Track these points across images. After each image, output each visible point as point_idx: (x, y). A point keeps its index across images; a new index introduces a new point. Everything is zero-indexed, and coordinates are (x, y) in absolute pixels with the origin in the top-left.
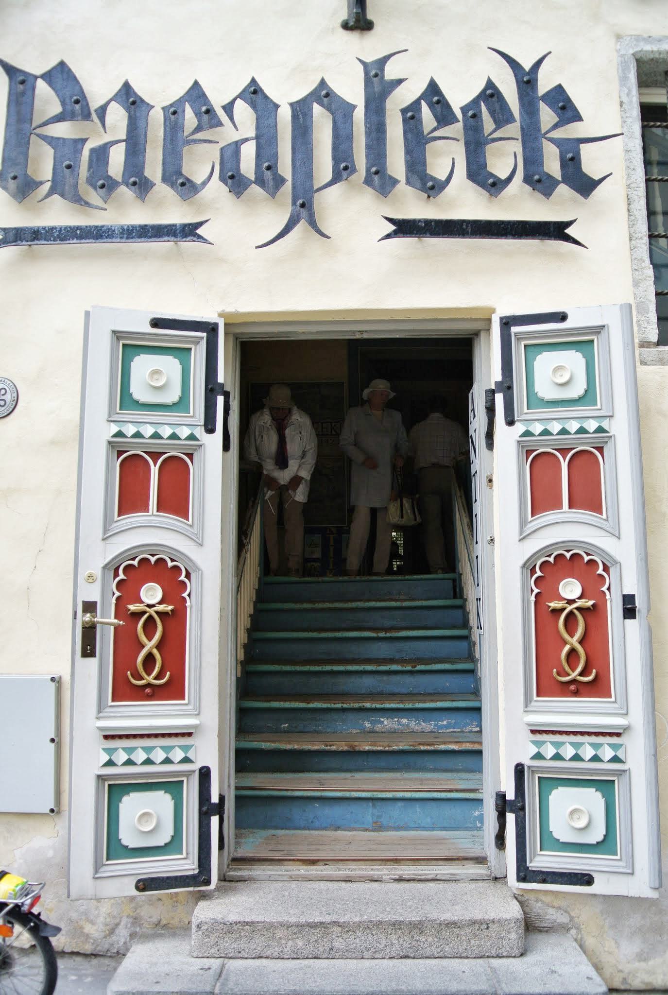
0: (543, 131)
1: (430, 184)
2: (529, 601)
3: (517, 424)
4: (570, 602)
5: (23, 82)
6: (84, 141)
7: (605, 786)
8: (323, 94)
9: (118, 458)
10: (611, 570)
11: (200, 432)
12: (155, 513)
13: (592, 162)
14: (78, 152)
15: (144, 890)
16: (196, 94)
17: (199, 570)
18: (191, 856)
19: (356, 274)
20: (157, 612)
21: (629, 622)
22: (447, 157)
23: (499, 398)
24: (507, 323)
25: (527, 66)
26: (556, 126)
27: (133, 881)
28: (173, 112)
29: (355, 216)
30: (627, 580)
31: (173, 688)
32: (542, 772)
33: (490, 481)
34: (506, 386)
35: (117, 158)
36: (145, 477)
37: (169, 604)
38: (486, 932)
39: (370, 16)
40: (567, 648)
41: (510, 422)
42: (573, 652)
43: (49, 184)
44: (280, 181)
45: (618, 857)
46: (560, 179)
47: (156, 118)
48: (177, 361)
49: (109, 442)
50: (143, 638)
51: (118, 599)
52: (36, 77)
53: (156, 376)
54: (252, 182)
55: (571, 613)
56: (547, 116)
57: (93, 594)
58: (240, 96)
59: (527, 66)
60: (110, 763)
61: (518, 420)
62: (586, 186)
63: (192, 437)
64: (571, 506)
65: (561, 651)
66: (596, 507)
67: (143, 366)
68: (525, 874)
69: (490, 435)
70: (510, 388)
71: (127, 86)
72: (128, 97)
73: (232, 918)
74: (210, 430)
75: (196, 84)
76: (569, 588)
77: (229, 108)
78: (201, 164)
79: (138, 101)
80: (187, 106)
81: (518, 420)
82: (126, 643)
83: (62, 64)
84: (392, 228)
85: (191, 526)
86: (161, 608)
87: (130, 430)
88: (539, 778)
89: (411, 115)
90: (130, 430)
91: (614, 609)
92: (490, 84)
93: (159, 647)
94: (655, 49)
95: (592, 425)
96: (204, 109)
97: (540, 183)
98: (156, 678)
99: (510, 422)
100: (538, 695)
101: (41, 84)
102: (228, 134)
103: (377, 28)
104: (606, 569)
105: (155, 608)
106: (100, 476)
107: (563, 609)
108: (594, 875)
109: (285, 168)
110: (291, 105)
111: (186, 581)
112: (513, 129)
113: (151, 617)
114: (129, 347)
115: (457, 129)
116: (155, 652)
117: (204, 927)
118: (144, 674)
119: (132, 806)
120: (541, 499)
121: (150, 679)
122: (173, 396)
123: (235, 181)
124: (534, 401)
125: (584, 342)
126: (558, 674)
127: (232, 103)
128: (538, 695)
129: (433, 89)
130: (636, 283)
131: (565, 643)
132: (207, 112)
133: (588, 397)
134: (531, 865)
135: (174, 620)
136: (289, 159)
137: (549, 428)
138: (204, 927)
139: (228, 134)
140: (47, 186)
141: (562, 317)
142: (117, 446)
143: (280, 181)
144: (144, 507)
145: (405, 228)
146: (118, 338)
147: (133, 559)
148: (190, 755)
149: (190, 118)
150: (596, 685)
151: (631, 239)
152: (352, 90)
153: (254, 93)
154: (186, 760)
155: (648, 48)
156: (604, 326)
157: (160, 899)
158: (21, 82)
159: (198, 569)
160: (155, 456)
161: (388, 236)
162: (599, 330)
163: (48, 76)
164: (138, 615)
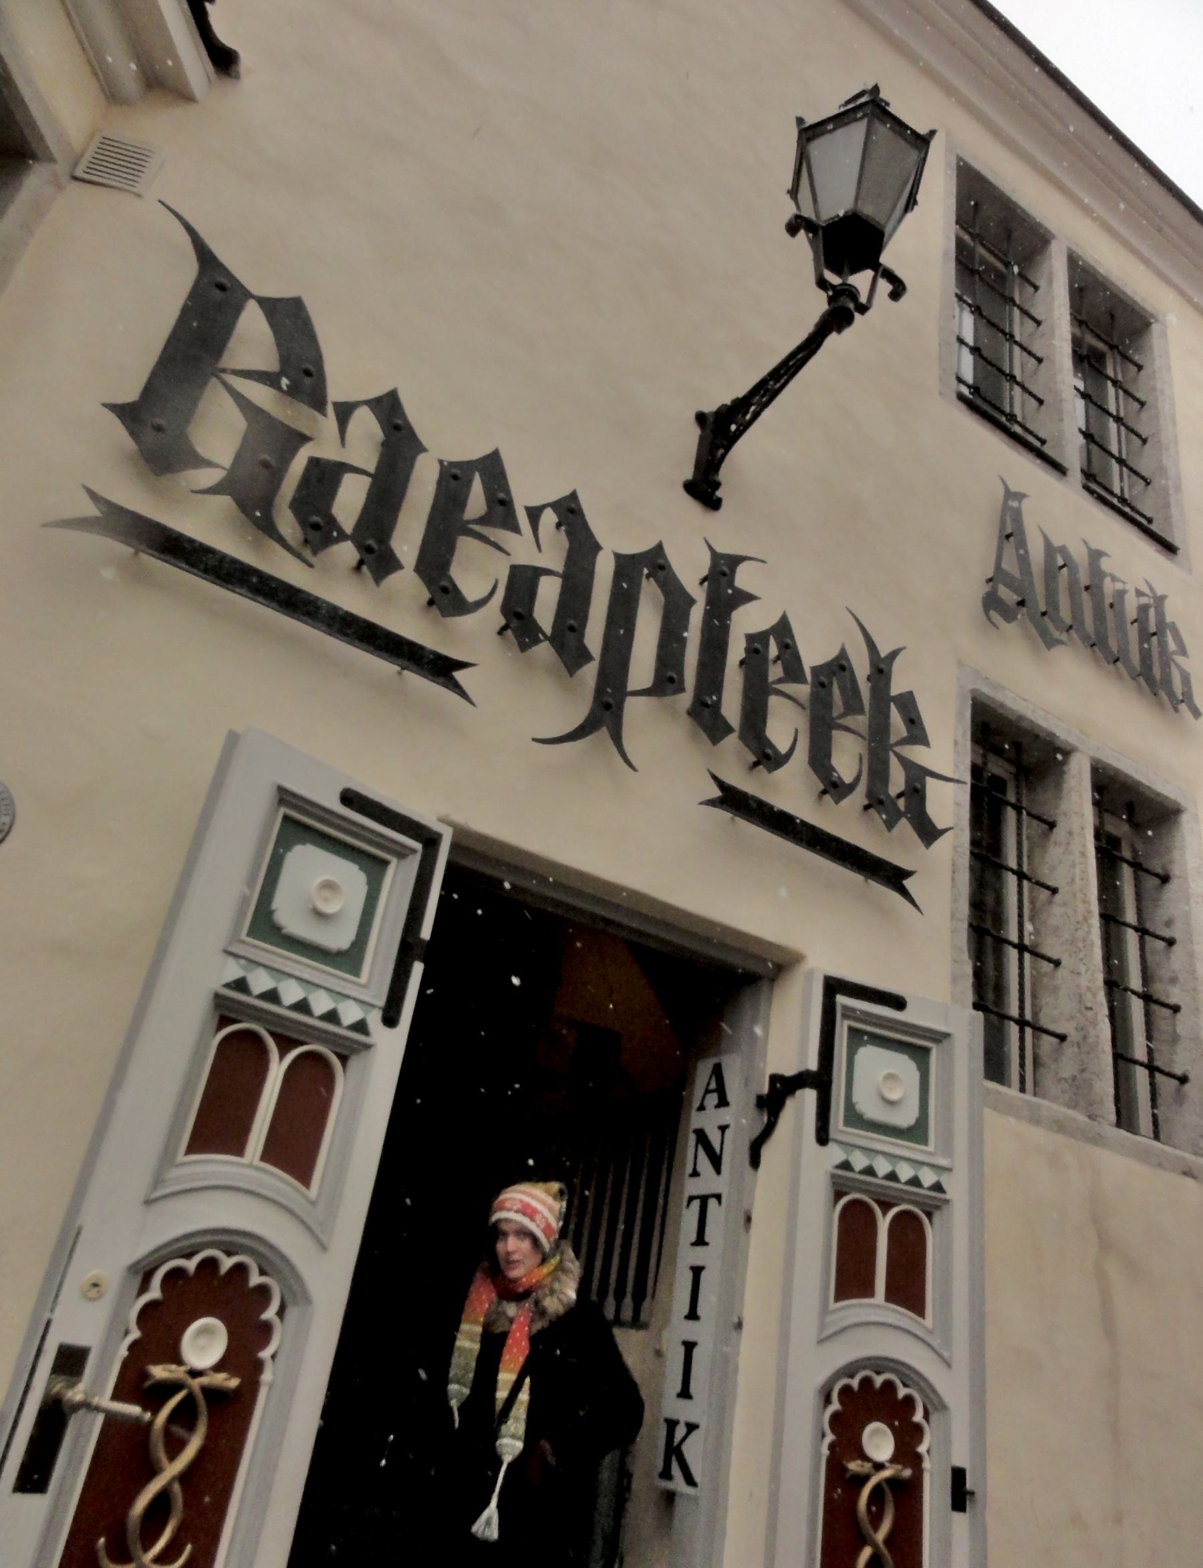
1: (316, 519)
3: (832, 1146)
4: (879, 1467)
6: (304, 439)
8: (655, 562)
9: (219, 1028)
11: (374, 1020)
12: (257, 1162)
14: (293, 451)
19: (637, 829)
21: (958, 1516)
22: (784, 725)
24: (833, 987)
26: (780, 681)
28: (454, 478)
33: (749, 1219)
35: (350, 499)
36: (252, 1083)
37: (233, 1374)
44: (583, 656)
47: (604, 568)
49: (217, 996)
50: (162, 1455)
52: (248, 295)
53: (327, 893)
54: (343, 536)
58: (367, 403)
61: (836, 1141)
63: (361, 1027)
64: (267, 1156)
65: (130, 1500)
74: (390, 1020)
77: (534, 514)
78: (477, 571)
81: (836, 1141)
82: (125, 1456)
84: (459, 675)
85: (313, 1203)
87: (260, 982)
90: (260, 982)
92: (843, 654)
93: (184, 1478)
102: (521, 549)
105: (204, 1380)
106: (174, 1058)
107: (865, 1478)
109: (594, 636)
110: (618, 557)
111: (276, 1321)
114: (298, 822)
115: (803, 691)
122: (340, 938)
123: (518, 621)
129: (783, 629)
133: (917, 1132)
135: (227, 1411)
139: (521, 549)
140: (208, 477)
141: (898, 1003)
142: (225, 1010)
143: (583, 656)
145: (733, 800)
147: (189, 1256)
149: (773, 650)
156: (947, 1035)
159: (308, 1300)
160: (285, 1044)
163: (270, 306)
164: (170, 1388)
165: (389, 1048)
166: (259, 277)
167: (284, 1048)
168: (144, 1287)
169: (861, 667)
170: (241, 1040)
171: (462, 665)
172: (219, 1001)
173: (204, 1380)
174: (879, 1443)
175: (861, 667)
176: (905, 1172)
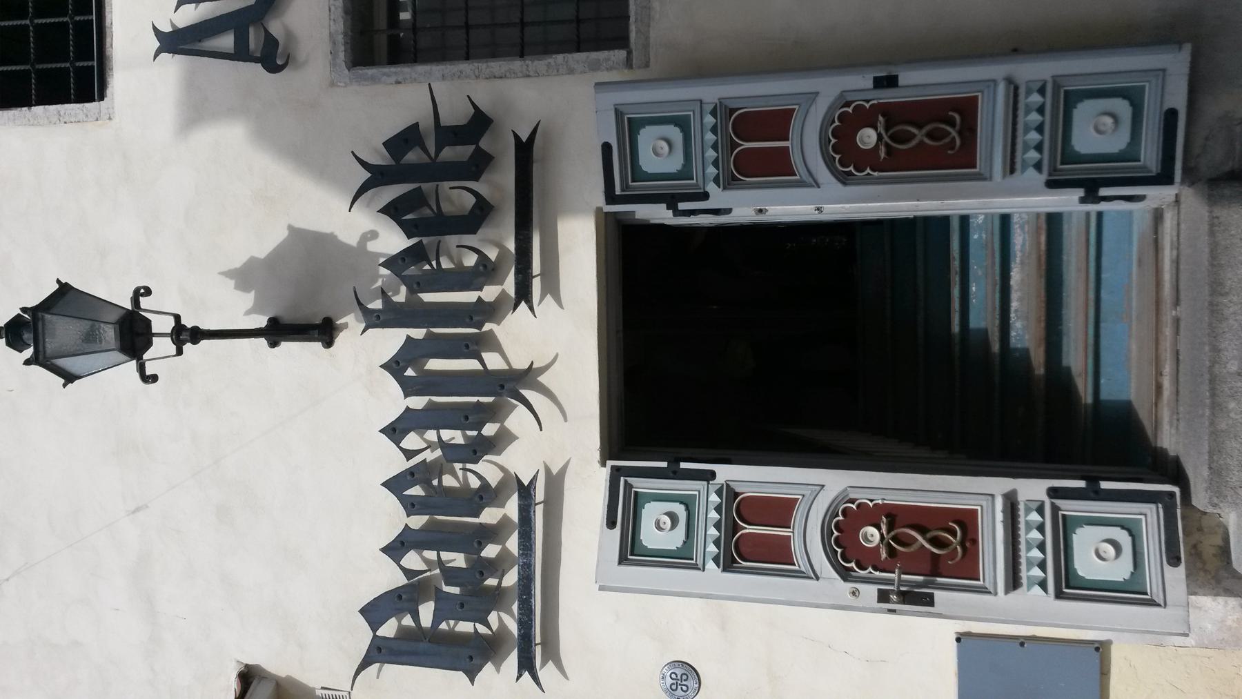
0: (428, 161)
2: (878, 178)
4: (880, 137)
5: (379, 649)
7: (1071, 100)
8: (394, 367)
10: (849, 99)
13: (455, 113)
15: (1179, 559)
16: (395, 485)
17: (846, 490)
18: (1144, 511)
19: (560, 335)
20: (888, 532)
21: (901, 82)
22: (461, 252)
23: (682, 206)
24: (611, 198)
25: (366, 175)
27: (1167, 567)
29: (521, 337)
30: (859, 82)
31: (966, 522)
32: (1055, 161)
34: (671, 201)
36: (753, 542)
38: (1222, 219)
39: (318, 321)
40: (927, 141)
41: (705, 196)
42: (930, 135)
43: (477, 625)
45: (1147, 85)
46: (474, 147)
47: (418, 402)
48: (647, 505)
50: (914, 143)
51: (875, 569)
52: (375, 636)
53: (660, 151)
55: (891, 137)
56: (413, 156)
57: (870, 591)
59: (366, 175)
60: (1043, 584)
62: (480, 122)
63: (719, 493)
64: (787, 139)
66: (786, 115)
67: (650, 537)
68: (1164, 178)
69: (716, 212)
70: (673, 196)
71: (385, 550)
72: (395, 550)
73: (1206, 472)
75: (384, 484)
76: (866, 140)
77: (409, 454)
79: (401, 539)
80: (408, 492)
83: (362, 611)
86: (884, 528)
88: (1062, 163)
89: (416, 285)
91: (888, 96)
94: (343, 48)
95: (709, 120)
96: (409, 477)
97: (479, 164)
98: (954, 535)
99: (705, 196)
100: (974, 167)
101: (380, 633)
103: (330, 314)
104: (848, 104)
108: (1166, 107)
110: (406, 396)
112: (427, 187)
113: (894, 539)
116: (928, 535)
117: (1216, 500)
118: (951, 547)
119: (1087, 565)
120: (776, 168)
121: (955, 541)
123: (479, 449)
124: (685, 173)
125: (629, 127)
126: (952, 148)
127: (404, 451)
128: (974, 167)
130: (571, 71)
131: (921, 143)
132: (412, 474)
133: (682, 123)
134: (1154, 169)
135: (893, 516)
136: (458, 397)
137: (710, 127)
138: (1216, 500)
141: (606, 148)
142: (728, 565)
144: (785, 542)
146: (627, 559)
148: (1035, 505)
149: (417, 491)
150: (964, 111)
151: (528, 76)
152: (392, 340)
153: (394, 431)
154: (1040, 510)
155: (342, 55)
156: (616, 111)
157: (1195, 546)
158: (379, 653)
160: (734, 145)
161: (531, 308)
162: (619, 114)
165: (726, 473)
166: (364, 636)
167: (736, 145)
168: (851, 569)
169: (390, 193)
170: (738, 554)
171: (517, 137)
172: (727, 569)
173: (883, 132)
174: (868, 137)
175: (390, 193)
176: (710, 137)
